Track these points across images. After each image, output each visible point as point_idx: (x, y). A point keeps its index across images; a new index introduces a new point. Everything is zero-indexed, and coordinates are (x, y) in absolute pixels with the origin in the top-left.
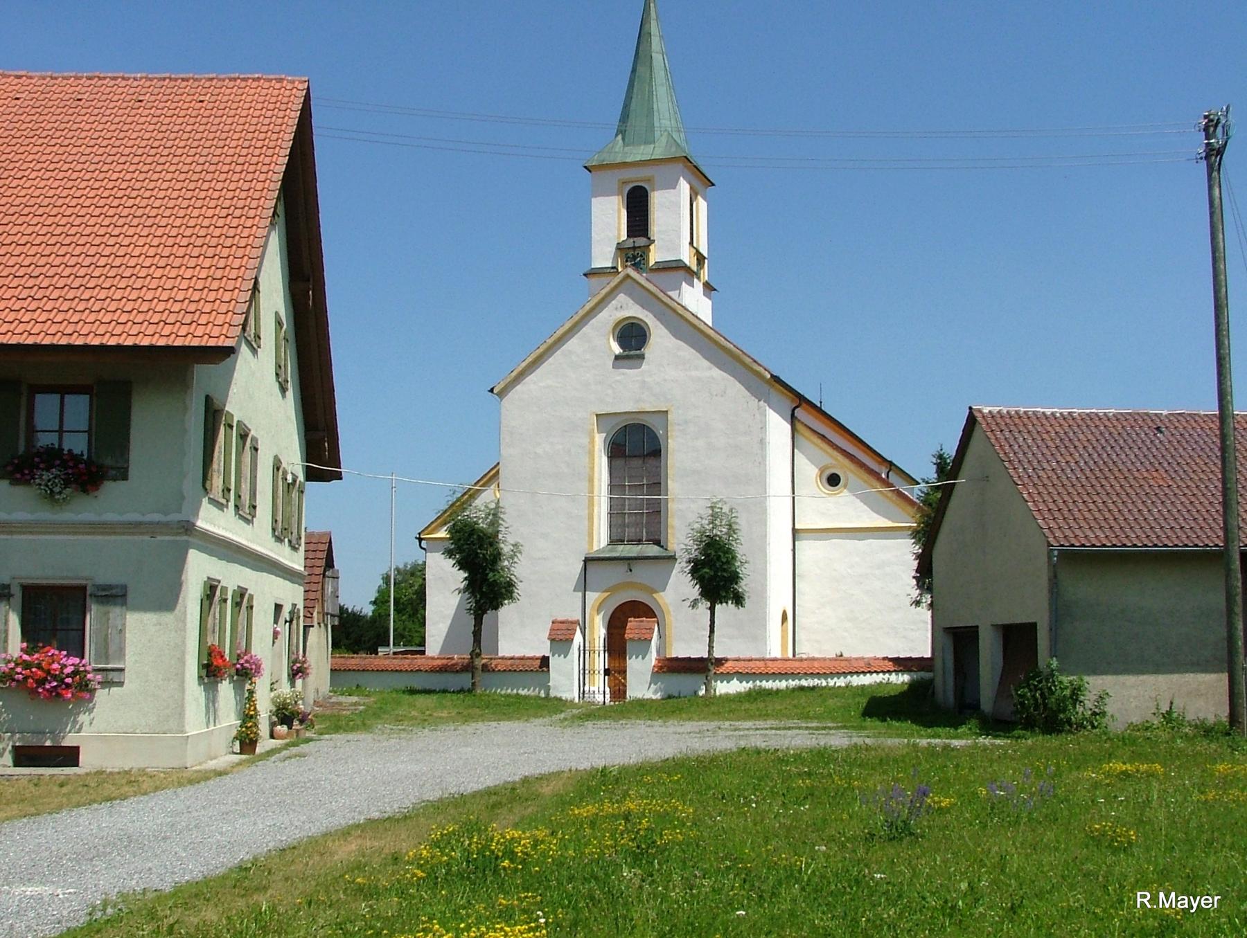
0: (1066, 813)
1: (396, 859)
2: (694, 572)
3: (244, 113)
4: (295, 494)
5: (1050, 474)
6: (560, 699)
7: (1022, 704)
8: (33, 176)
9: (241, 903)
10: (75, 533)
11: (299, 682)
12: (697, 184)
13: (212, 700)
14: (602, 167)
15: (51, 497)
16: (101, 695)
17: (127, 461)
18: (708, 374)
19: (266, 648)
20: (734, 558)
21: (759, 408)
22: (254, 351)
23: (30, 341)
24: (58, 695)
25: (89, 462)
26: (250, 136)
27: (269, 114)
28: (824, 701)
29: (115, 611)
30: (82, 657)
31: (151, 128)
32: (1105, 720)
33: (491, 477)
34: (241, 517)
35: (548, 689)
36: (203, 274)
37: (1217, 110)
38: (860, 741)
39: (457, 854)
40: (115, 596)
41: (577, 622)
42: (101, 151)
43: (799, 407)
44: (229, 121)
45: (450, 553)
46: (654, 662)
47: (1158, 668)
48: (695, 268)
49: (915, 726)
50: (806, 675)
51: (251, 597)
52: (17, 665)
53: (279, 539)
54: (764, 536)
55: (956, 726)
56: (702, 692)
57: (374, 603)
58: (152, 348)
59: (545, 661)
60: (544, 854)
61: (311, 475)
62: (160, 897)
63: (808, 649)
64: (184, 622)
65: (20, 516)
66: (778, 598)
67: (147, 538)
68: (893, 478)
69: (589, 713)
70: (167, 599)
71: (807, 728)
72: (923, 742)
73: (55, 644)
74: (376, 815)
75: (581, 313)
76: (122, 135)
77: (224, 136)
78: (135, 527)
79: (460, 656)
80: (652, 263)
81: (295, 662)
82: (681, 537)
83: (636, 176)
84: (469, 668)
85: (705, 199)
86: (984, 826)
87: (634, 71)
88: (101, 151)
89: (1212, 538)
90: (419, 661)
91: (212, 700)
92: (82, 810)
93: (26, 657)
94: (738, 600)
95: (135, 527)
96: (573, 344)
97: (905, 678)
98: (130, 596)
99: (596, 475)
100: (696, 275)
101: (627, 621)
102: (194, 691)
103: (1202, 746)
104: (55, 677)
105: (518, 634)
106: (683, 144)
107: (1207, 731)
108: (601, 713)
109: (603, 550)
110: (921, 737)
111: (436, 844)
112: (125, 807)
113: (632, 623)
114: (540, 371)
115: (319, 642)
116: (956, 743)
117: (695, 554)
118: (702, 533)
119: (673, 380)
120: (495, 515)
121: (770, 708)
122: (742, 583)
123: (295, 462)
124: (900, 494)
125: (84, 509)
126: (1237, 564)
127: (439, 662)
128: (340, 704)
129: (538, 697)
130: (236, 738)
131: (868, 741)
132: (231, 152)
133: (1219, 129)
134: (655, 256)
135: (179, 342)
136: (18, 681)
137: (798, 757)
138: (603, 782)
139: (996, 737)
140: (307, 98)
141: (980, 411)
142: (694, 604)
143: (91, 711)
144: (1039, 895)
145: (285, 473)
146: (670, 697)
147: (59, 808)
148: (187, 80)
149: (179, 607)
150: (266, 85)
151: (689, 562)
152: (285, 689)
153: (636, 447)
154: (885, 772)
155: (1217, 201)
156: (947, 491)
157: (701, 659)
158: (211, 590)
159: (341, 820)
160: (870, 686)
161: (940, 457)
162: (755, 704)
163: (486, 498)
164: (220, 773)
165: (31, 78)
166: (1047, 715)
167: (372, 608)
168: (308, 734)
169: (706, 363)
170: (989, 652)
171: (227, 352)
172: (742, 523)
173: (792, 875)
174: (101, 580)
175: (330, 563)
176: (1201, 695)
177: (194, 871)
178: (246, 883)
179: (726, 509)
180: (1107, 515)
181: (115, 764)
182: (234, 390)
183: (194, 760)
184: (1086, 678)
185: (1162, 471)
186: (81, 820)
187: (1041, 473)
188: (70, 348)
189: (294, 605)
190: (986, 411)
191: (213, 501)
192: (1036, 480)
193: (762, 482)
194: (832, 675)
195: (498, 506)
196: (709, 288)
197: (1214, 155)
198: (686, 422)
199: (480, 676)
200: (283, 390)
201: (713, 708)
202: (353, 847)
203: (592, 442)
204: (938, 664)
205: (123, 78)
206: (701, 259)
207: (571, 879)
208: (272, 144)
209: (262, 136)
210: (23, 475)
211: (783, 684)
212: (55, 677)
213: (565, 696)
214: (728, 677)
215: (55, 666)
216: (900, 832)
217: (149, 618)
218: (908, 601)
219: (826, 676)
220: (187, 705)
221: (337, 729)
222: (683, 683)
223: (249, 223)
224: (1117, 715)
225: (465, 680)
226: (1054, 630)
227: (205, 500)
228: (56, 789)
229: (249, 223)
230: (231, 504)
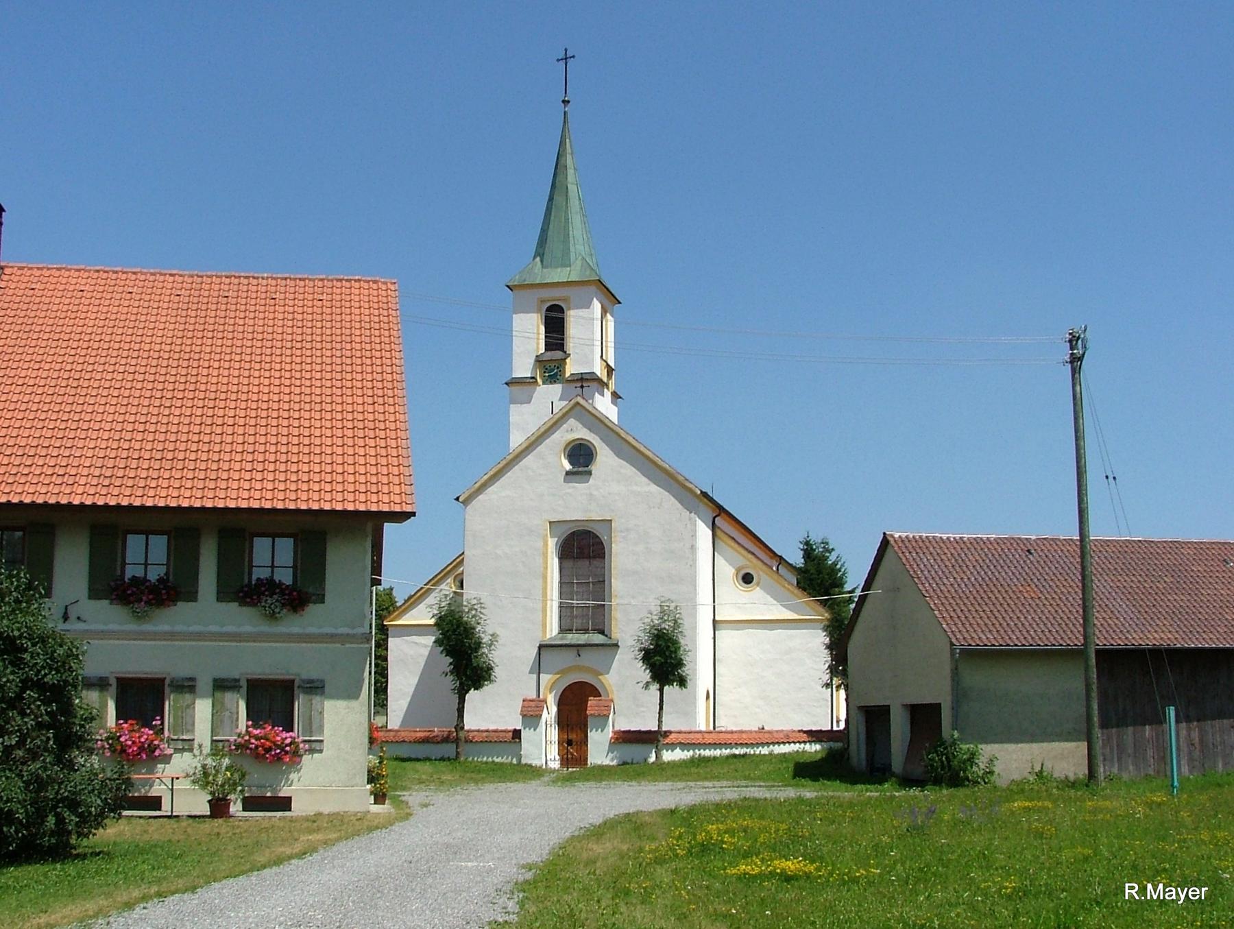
5: (950, 588)
6: (530, 766)
7: (932, 766)
12: (607, 303)
16: (306, 759)
18: (646, 489)
29: (316, 700)
32: (993, 778)
35: (520, 758)
40: (315, 688)
43: (718, 515)
46: (611, 735)
47: (1032, 738)
48: (605, 379)
50: (737, 745)
56: (653, 758)
59: (517, 734)
63: (725, 723)
65: (248, 628)
78: (332, 638)
80: (567, 375)
83: (553, 296)
87: (551, 199)
89: (1075, 639)
94: (682, 682)
95: (332, 638)
96: (529, 460)
98: (327, 689)
104: (278, 747)
105: (486, 711)
107: (1073, 785)
109: (554, 638)
114: (504, 480)
117: (646, 645)
119: (616, 494)
125: (293, 624)
126: (1093, 661)
129: (511, 764)
134: (571, 368)
141: (892, 536)
142: (647, 685)
143: (299, 771)
146: (625, 763)
151: (641, 650)
153: (583, 549)
161: (807, 543)
162: (696, 769)
166: (953, 775)
169: (645, 480)
170: (899, 726)
174: (304, 676)
176: (1065, 758)
179: (672, 606)
184: (980, 746)
187: (943, 587)
190: (896, 536)
194: (758, 745)
196: (616, 396)
197: (1076, 362)
198: (628, 530)
199: (463, 748)
203: (546, 545)
211: (717, 753)
213: (535, 763)
214: (672, 746)
217: (341, 704)
219: (752, 745)
222: (633, 751)
225: (449, 750)
226: (955, 708)
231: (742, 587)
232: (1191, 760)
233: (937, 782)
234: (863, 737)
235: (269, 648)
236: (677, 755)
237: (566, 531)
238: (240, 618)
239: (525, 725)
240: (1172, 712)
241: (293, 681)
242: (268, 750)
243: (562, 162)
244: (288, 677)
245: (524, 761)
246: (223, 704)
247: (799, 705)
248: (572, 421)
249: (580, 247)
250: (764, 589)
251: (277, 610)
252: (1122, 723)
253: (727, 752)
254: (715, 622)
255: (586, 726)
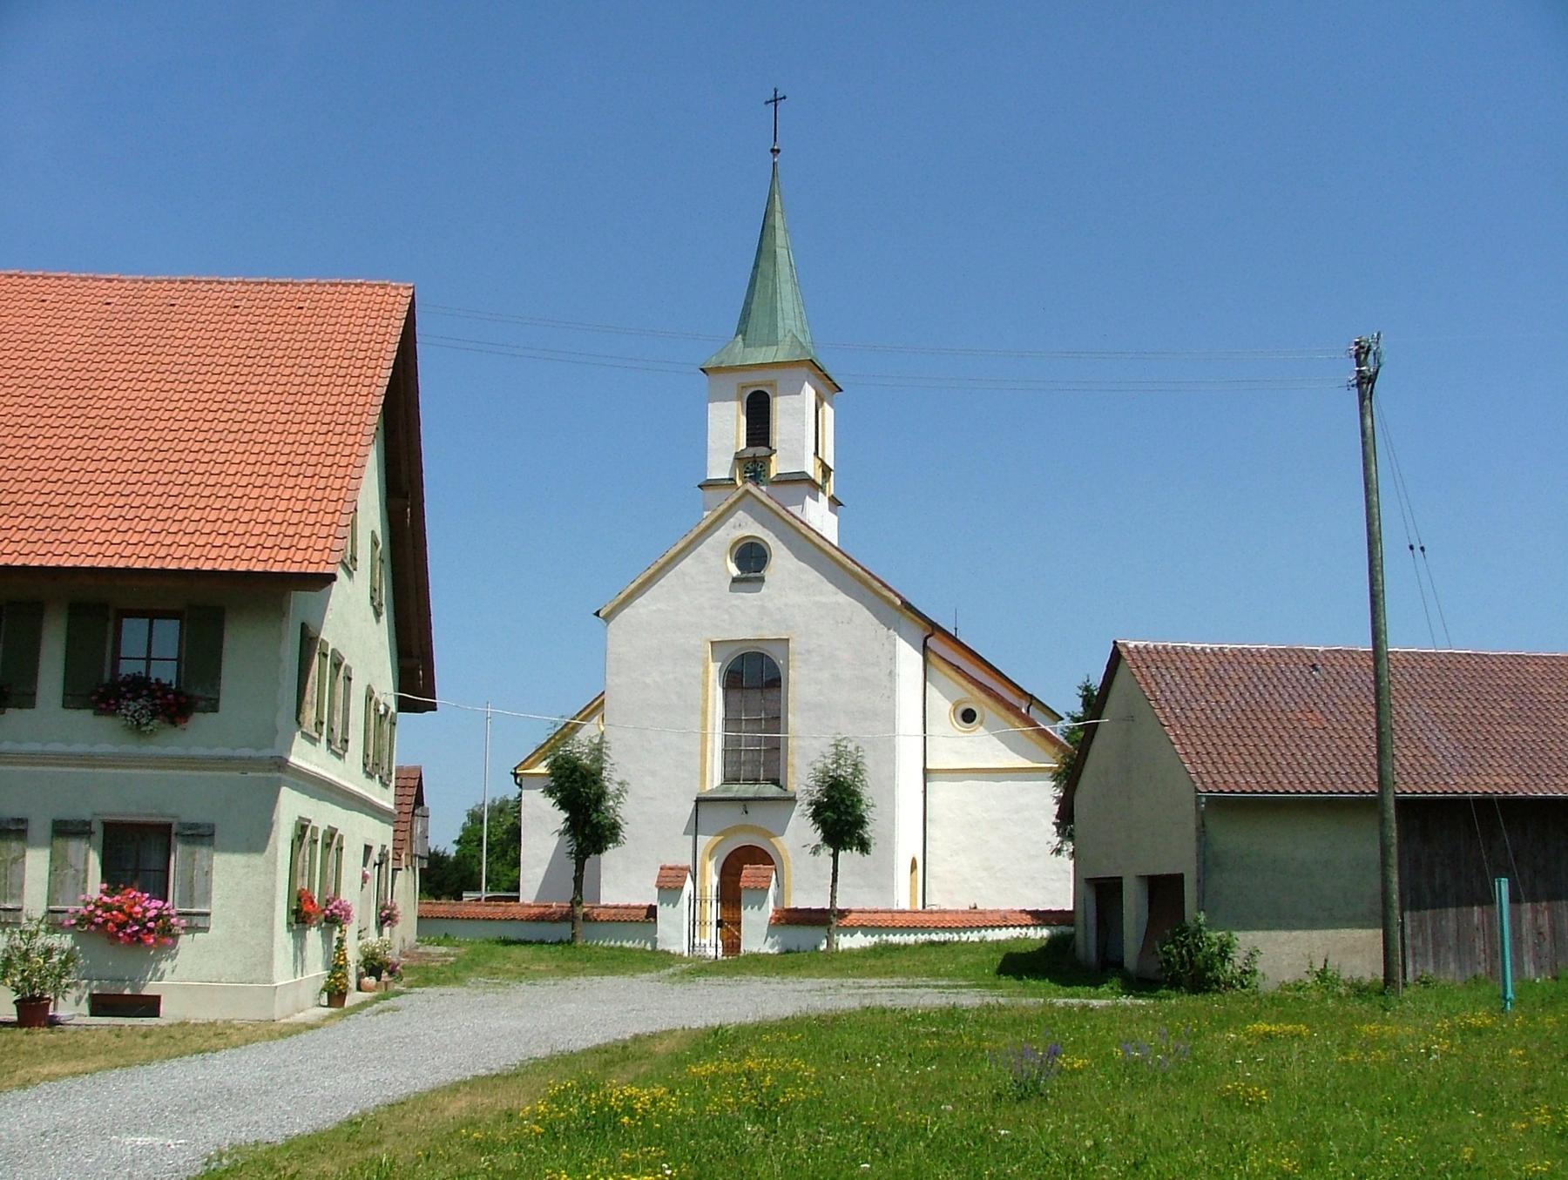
0: (1202, 1074)
1: (510, 1116)
2: (816, 816)
3: (346, 321)
4: (386, 726)
5: (1199, 714)
6: (668, 953)
7: (1167, 961)
8: (124, 386)
9: (356, 1155)
10: (164, 768)
11: (386, 930)
12: (824, 391)
13: (300, 947)
14: (718, 369)
15: (137, 729)
16: (185, 940)
17: (218, 693)
19: (354, 893)
20: (860, 801)
21: (888, 637)
22: (350, 574)
23: (121, 564)
24: (140, 940)
25: (177, 693)
26: (351, 346)
27: (372, 322)
28: (956, 957)
29: (201, 852)
30: (166, 900)
31: (247, 336)
32: (1255, 980)
33: (595, 708)
34: (333, 752)
35: (655, 942)
36: (302, 495)
37: (1367, 336)
38: (992, 1001)
39: (574, 1110)
40: (201, 835)
41: (687, 869)
42: (195, 360)
43: (934, 638)
44: (330, 329)
45: (550, 792)
46: (771, 913)
47: (1312, 924)
48: (819, 480)
49: (1052, 985)
51: (341, 837)
52: (97, 907)
53: (370, 776)
54: (892, 777)
55: (1096, 985)
56: (823, 947)
57: (458, 842)
58: (248, 574)
59: (652, 911)
60: (664, 1111)
61: (404, 705)
62: (273, 1149)
63: (937, 900)
64: (275, 863)
66: (907, 845)
67: (237, 774)
68: (1035, 713)
69: (700, 968)
70: (256, 840)
71: (936, 987)
72: (1060, 1002)
73: (136, 885)
74: (482, 1072)
75: (696, 531)
76: (217, 343)
77: (324, 345)
78: (225, 762)
79: (559, 904)
80: (773, 475)
81: (384, 908)
82: (802, 778)
83: (757, 380)
84: (568, 917)
85: (831, 405)
86: (1116, 1087)
87: (756, 266)
88: (195, 360)
89: (1366, 784)
90: (513, 909)
91: (300, 947)
92: (175, 1062)
93: (106, 899)
94: (864, 846)
95: (225, 762)
96: (687, 564)
97: (1044, 933)
99: (710, 709)
100: (822, 488)
101: (742, 868)
102: (283, 938)
103: (1357, 1007)
104: (136, 921)
105: (622, 880)
106: (809, 346)
107: (1360, 990)
108: (714, 968)
110: (1059, 996)
111: (553, 1099)
112: (218, 1059)
113: (748, 870)
114: (654, 591)
115: (406, 889)
116: (1095, 1003)
117: (817, 796)
118: (825, 772)
119: (795, 605)
120: (598, 751)
121: (897, 965)
122: (868, 828)
123: (387, 692)
124: (1043, 733)
127: (536, 911)
128: (428, 954)
130: (324, 990)
131: (1001, 1000)
132: (332, 363)
133: (1371, 357)
134: (776, 467)
135: (277, 568)
136: (97, 924)
137: (926, 1016)
138: (716, 1040)
139: (1137, 997)
140: (412, 305)
141: (1125, 645)
142: (816, 850)
143: (173, 958)
144: (1165, 1152)
145: (377, 703)
146: (788, 952)
147: (149, 1061)
148: (286, 285)
149: (269, 848)
150: (369, 291)
151: (810, 804)
152: (372, 938)
153: (754, 677)
154: (1018, 1033)
155: (1369, 431)
156: (1091, 731)
157: (823, 911)
158: (302, 828)
159: (447, 1076)
160: (1006, 941)
161: (1087, 689)
163: (589, 732)
164: (312, 1027)
165: (123, 281)
166: (1196, 975)
167: (456, 847)
168: (397, 987)
169: (831, 587)
170: (1134, 905)
171: (333, 577)
172: (869, 763)
173: (917, 1132)
174: (186, 819)
175: (419, 801)
176: (1356, 951)
177: (301, 1125)
178: (360, 1137)
179: (851, 747)
180: (1259, 759)
181: (200, 1014)
182: (329, 616)
183: (282, 1011)
184: (1235, 934)
185: (1317, 712)
186: (175, 1072)
187: (1189, 713)
188: (163, 572)
189: (384, 847)
190: (1131, 645)
191: (306, 736)
192: (1184, 721)
193: (890, 718)
194: (965, 929)
195: (602, 741)
196: (835, 502)
197: (1365, 383)
198: (809, 652)
199: (581, 927)
200: (378, 614)
201: (836, 964)
202: (463, 1104)
203: (706, 671)
204: (1079, 918)
205: (219, 283)
206: (826, 471)
207: (693, 1135)
208: (375, 355)
209: (364, 346)
210: (109, 705)
211: (911, 939)
212: (136, 921)
213: (673, 949)
214: (851, 930)
215: (137, 909)
216: (1028, 1092)
217: (238, 860)
218: (1049, 849)
219: (957, 930)
220: (276, 954)
221: (427, 982)
222: (801, 936)
223: (350, 440)
224: (1268, 974)
225: (564, 930)
226: (1201, 882)
227: (298, 734)
228: (139, 1040)
229: (350, 440)
230: (324, 739)
231: (960, 727)
232: (1537, 957)
233: (1175, 984)
234: (1092, 921)
235: (135, 775)
236: (859, 941)
237: (733, 653)
238: (92, 732)
239: (662, 900)
240: (1504, 886)
241: (170, 825)
242: (122, 926)
243: (770, 222)
244: (163, 820)
245: (660, 947)
246: (65, 858)
247: (1033, 878)
248: (740, 514)
249: (790, 322)
250: (989, 729)
251: (144, 721)
252: (1439, 902)
253: (922, 938)
254: (926, 771)
255: (739, 901)
